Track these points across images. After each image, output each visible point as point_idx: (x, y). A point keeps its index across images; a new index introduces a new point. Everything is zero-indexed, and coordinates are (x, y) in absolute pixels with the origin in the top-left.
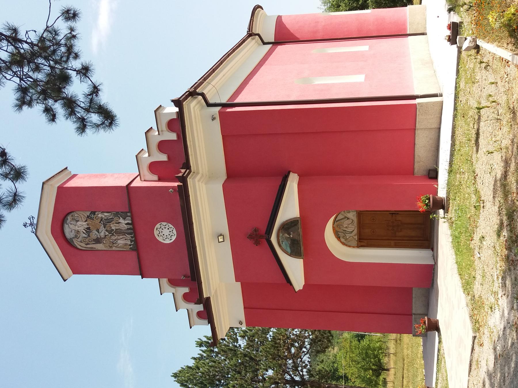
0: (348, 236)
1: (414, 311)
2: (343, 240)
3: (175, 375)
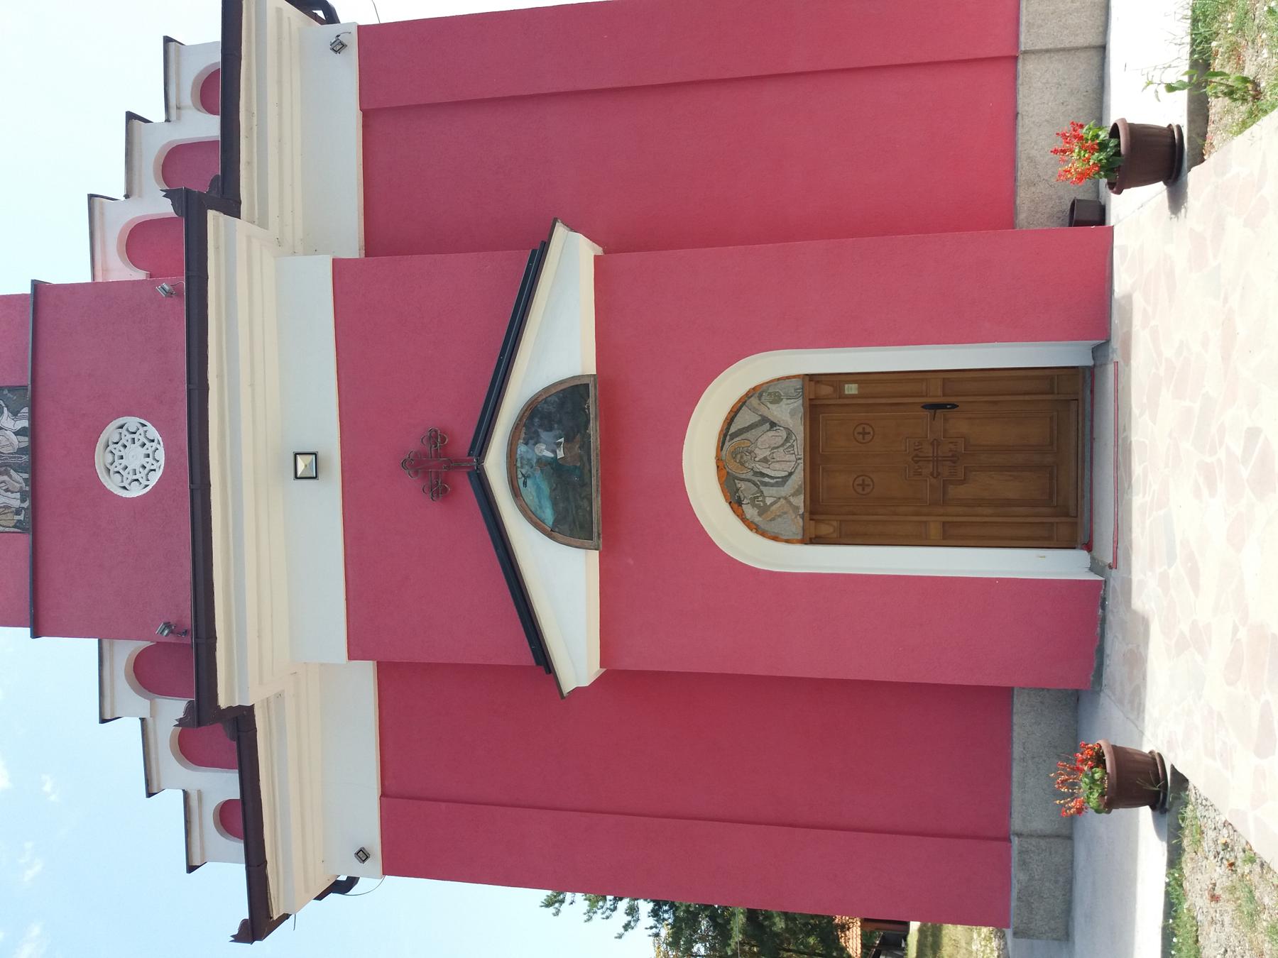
0: (770, 494)
1: (1016, 823)
2: (750, 512)
3: (238, 938)
